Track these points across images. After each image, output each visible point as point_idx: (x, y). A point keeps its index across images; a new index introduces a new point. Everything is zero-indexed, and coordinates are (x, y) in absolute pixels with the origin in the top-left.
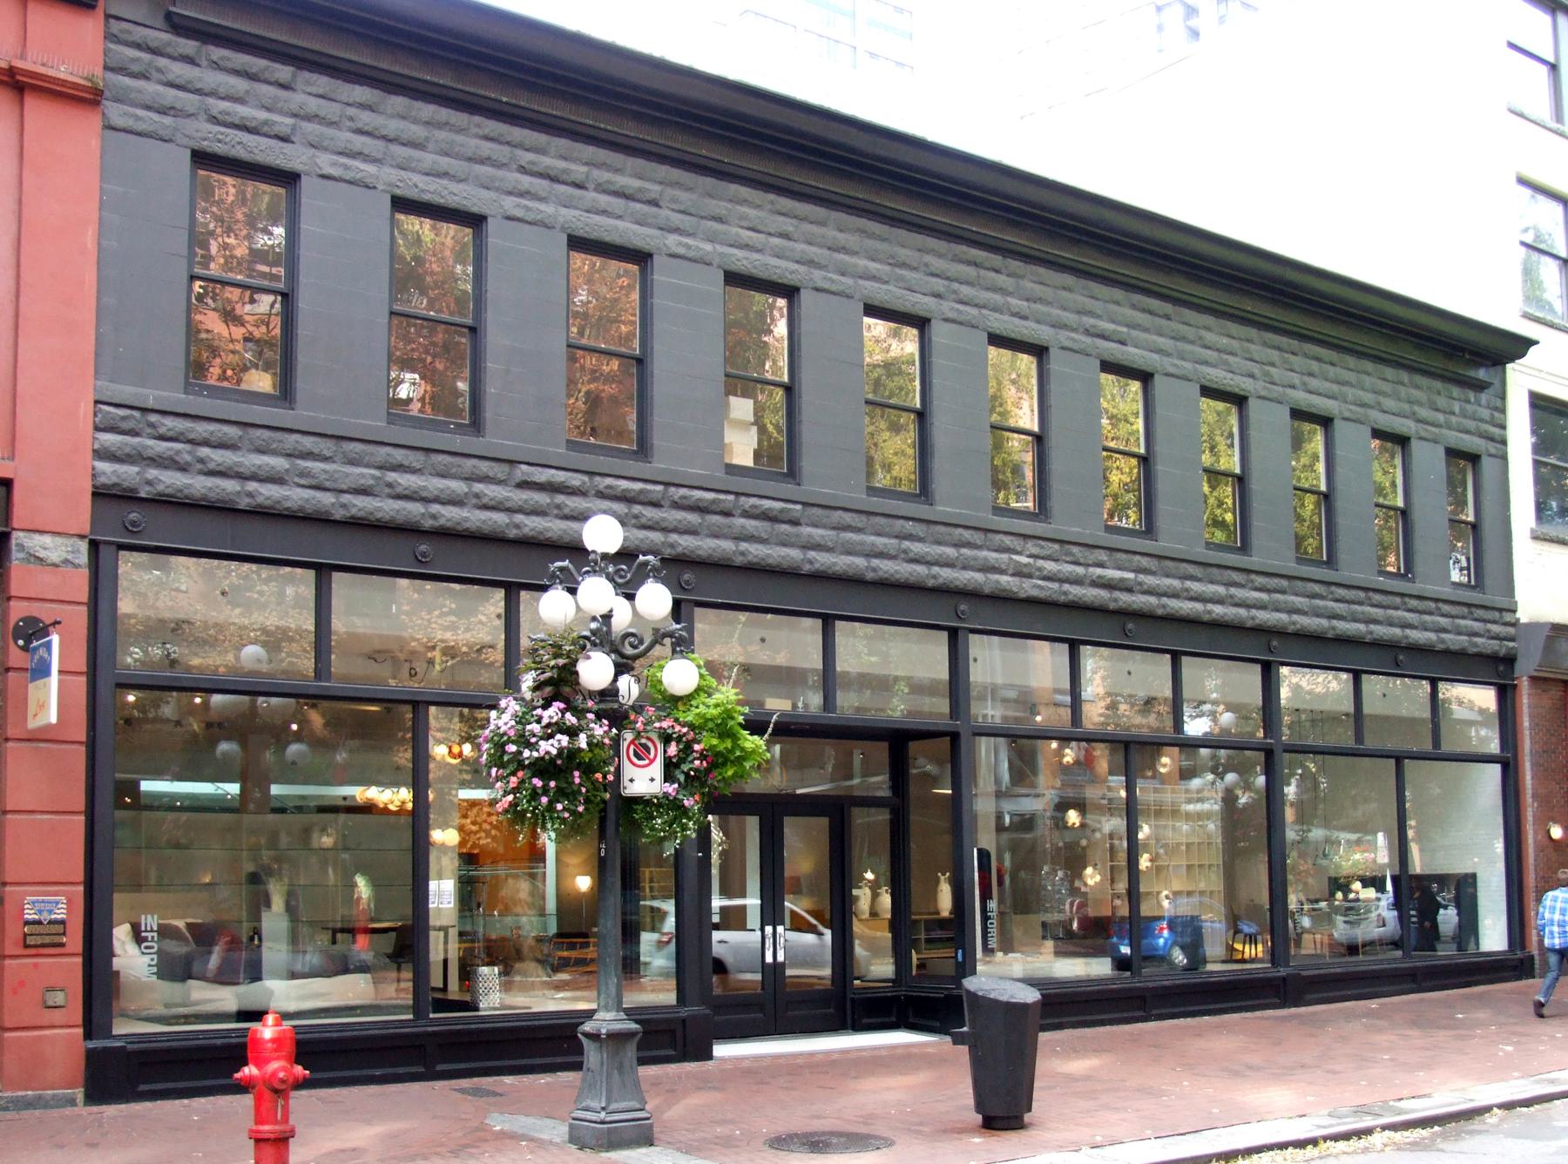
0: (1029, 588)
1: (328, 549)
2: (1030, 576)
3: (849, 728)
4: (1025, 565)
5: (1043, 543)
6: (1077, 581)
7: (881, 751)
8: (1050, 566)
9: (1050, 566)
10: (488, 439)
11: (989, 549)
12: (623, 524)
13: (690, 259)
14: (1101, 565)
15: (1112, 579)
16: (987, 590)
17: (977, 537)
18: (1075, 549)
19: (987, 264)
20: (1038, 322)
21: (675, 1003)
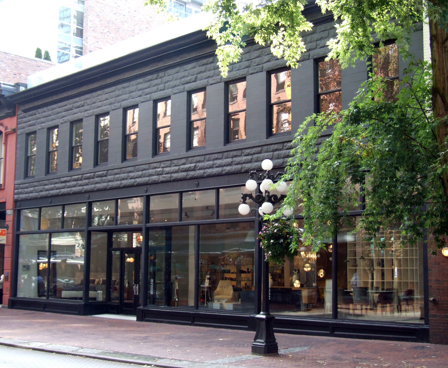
0: (161, 178)
1: (179, 187)
2: (162, 174)
3: (123, 229)
4: (160, 171)
5: (165, 162)
6: (52, 189)
7: (163, 234)
8: (167, 169)
9: (167, 169)
10: (109, 166)
11: (151, 169)
12: (271, 159)
13: (256, 73)
14: (184, 164)
15: (186, 168)
16: (39, 197)
17: (146, 167)
18: (175, 161)
19: (153, 78)
20: (81, 112)
21: (232, 309)
